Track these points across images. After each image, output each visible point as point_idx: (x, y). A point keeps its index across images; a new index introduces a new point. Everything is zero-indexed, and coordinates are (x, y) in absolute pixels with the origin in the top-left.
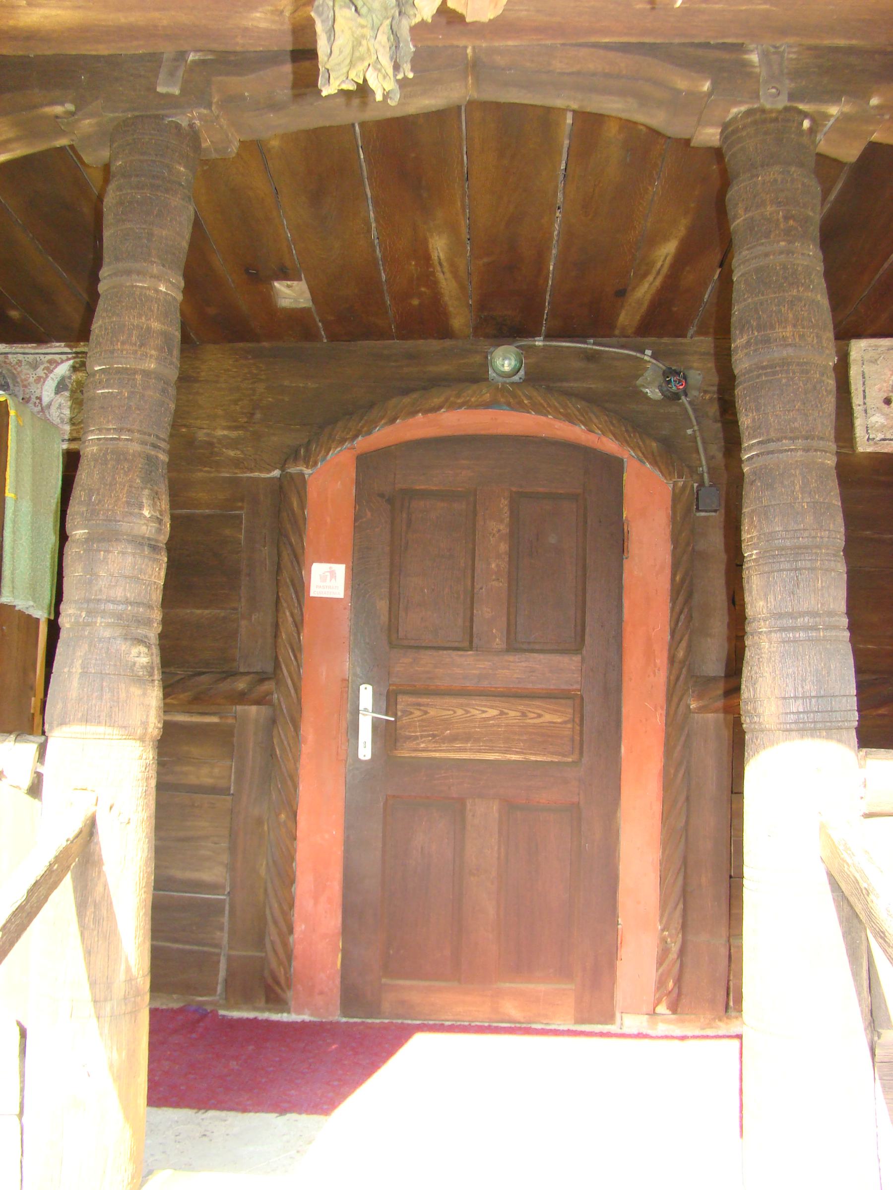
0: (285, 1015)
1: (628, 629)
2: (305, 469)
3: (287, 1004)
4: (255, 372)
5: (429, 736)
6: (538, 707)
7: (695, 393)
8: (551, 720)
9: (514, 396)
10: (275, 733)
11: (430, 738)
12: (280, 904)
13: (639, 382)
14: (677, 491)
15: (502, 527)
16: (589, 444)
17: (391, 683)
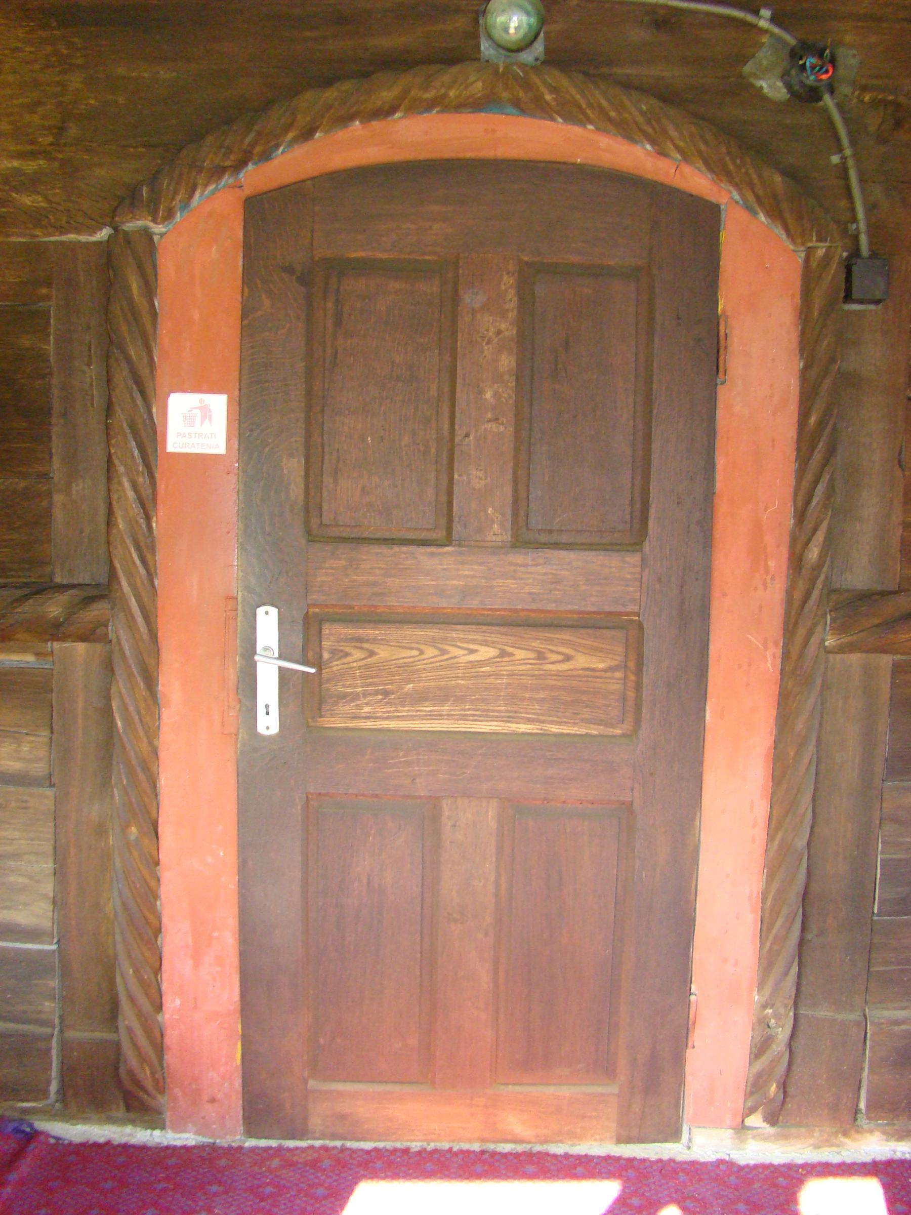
0: (157, 1133)
1: (722, 508)
2: (151, 224)
3: (160, 1113)
4: (65, 52)
5: (377, 693)
6: (564, 643)
7: (845, 90)
8: (587, 666)
9: (527, 86)
10: (114, 690)
11: (380, 697)
12: (137, 971)
13: (747, 69)
14: (814, 264)
15: (503, 326)
16: (661, 178)
17: (310, 602)
